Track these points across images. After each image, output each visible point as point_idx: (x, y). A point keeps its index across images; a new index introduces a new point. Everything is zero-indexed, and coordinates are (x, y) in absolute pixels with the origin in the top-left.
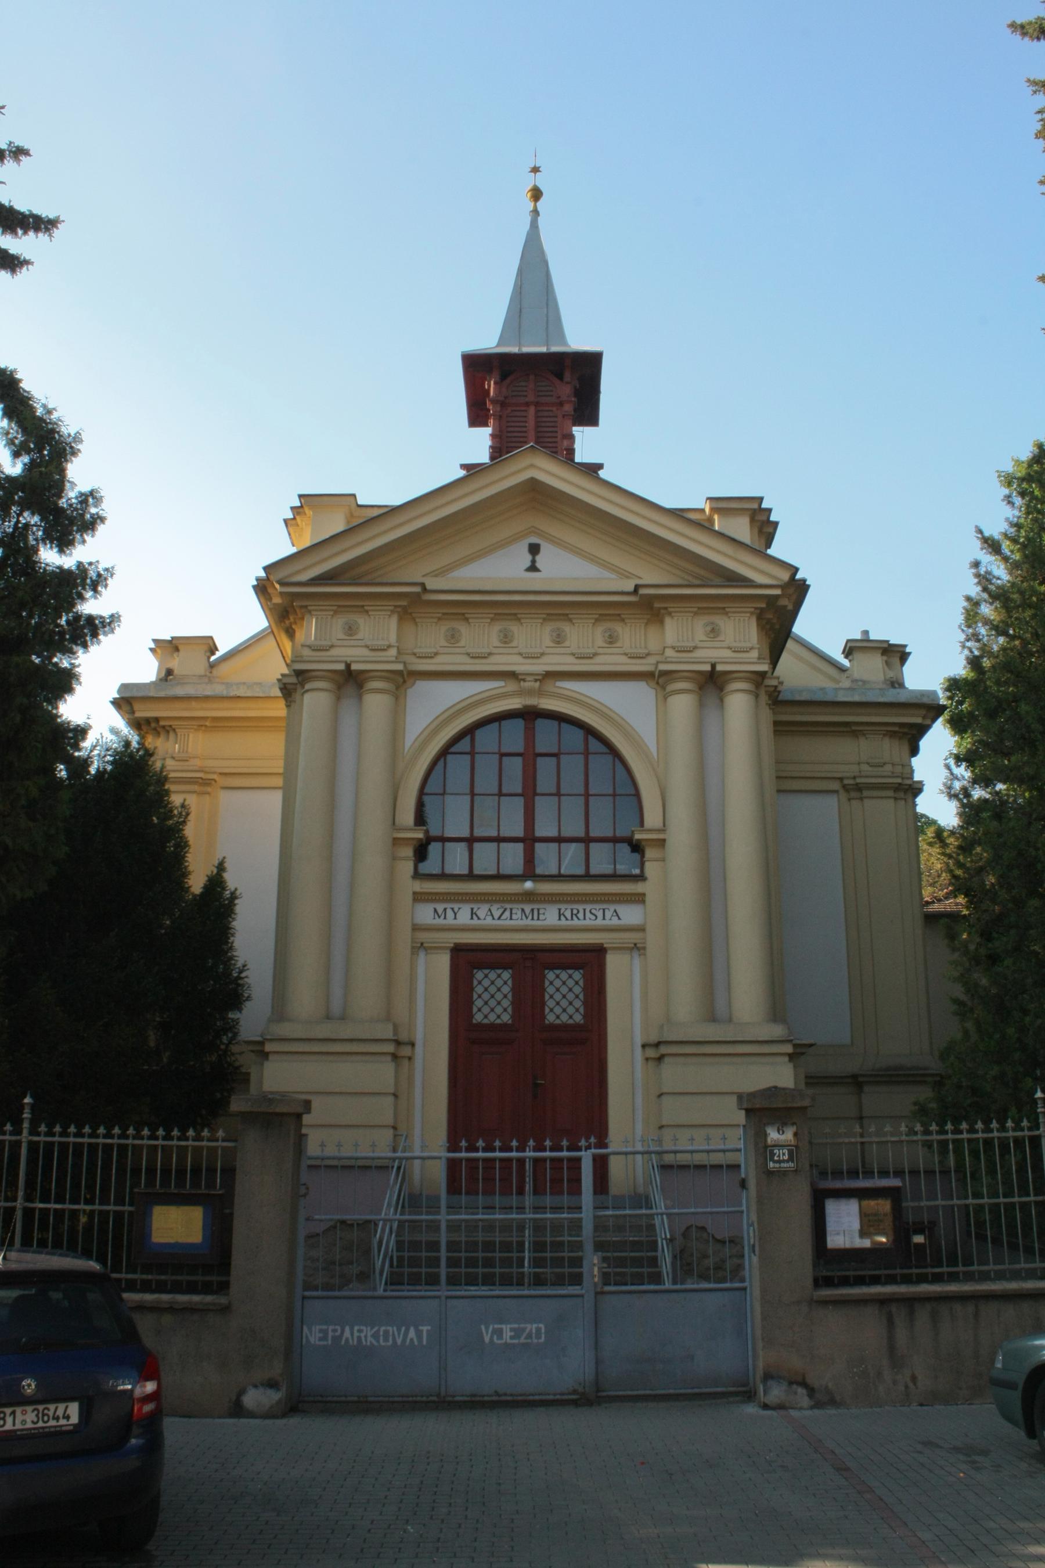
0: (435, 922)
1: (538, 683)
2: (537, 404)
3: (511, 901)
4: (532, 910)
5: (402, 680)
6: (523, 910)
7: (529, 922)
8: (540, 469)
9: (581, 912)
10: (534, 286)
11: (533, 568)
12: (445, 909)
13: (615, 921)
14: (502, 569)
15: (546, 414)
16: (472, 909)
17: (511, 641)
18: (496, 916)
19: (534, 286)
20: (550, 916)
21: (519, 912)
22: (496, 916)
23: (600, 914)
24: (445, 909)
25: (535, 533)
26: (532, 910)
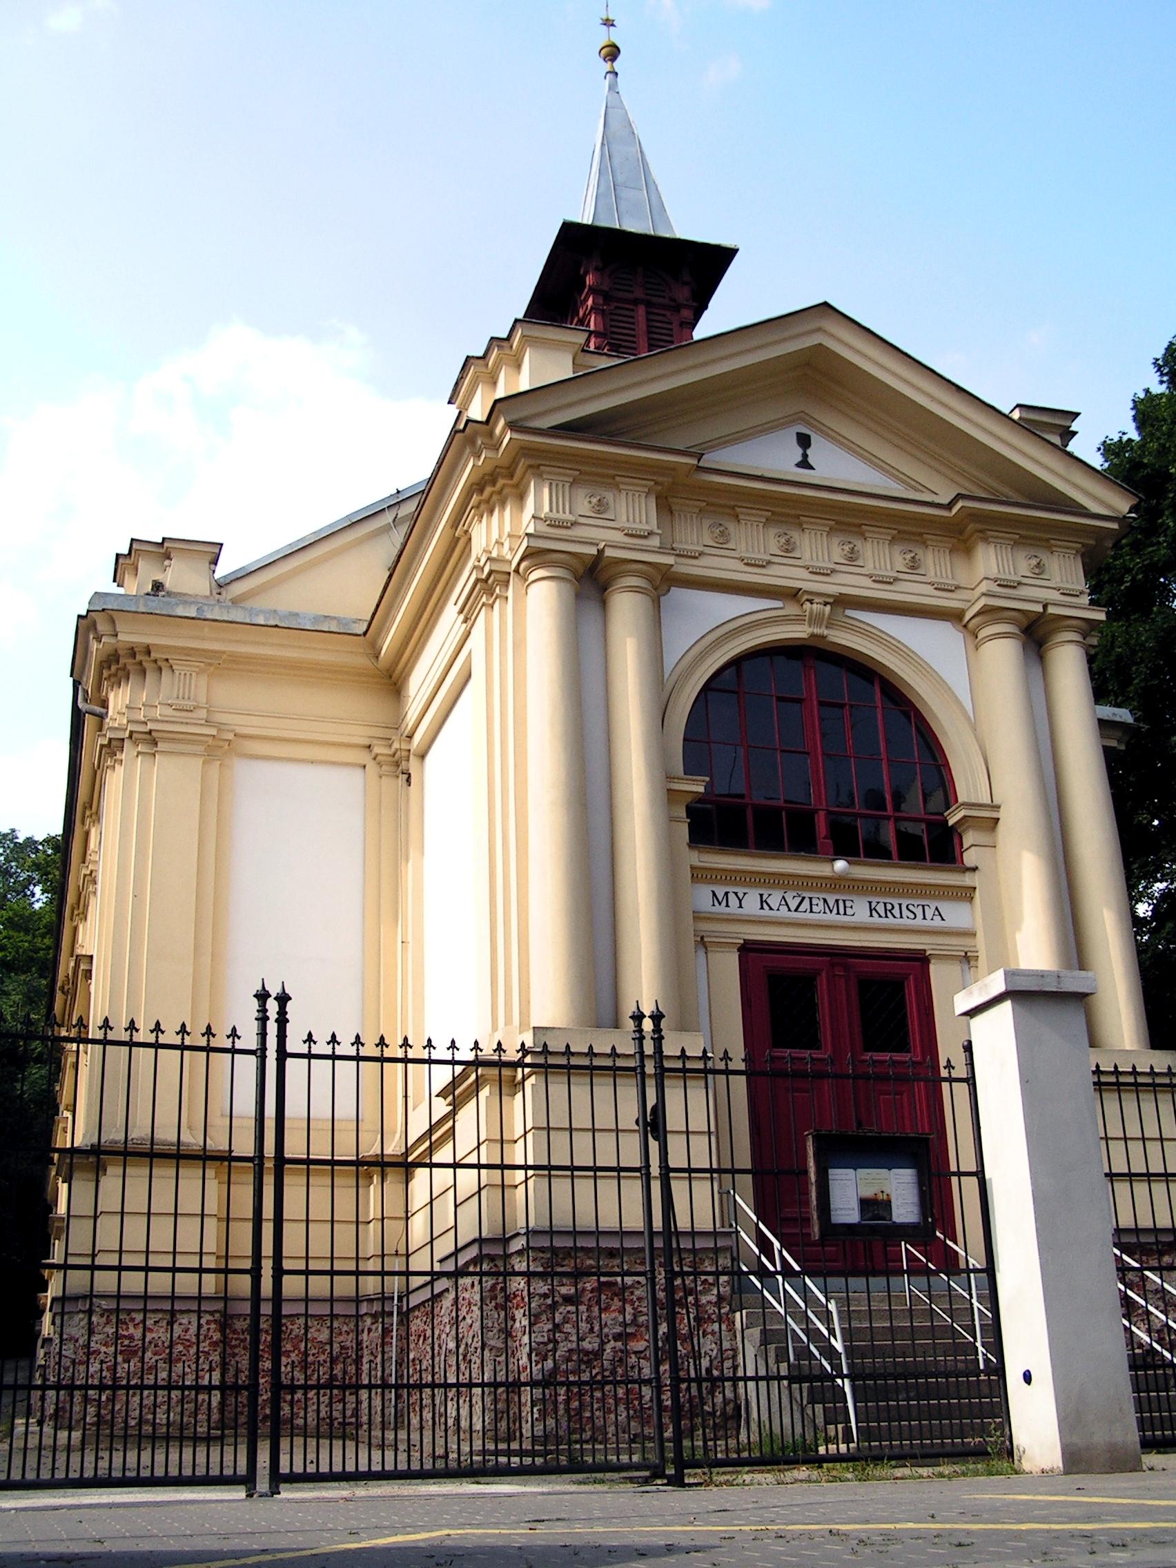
0: (713, 909)
1: (828, 608)
2: (648, 304)
3: (811, 889)
4: (837, 901)
5: (661, 582)
6: (825, 900)
7: (832, 917)
8: (832, 336)
9: (897, 907)
10: (621, 154)
11: (804, 464)
12: (726, 894)
13: (937, 922)
14: (773, 457)
15: (660, 318)
16: (761, 895)
17: (793, 550)
18: (793, 908)
19: (621, 154)
20: (859, 911)
21: (821, 903)
22: (793, 908)
23: (919, 911)
24: (726, 894)
25: (800, 419)
26: (837, 901)
